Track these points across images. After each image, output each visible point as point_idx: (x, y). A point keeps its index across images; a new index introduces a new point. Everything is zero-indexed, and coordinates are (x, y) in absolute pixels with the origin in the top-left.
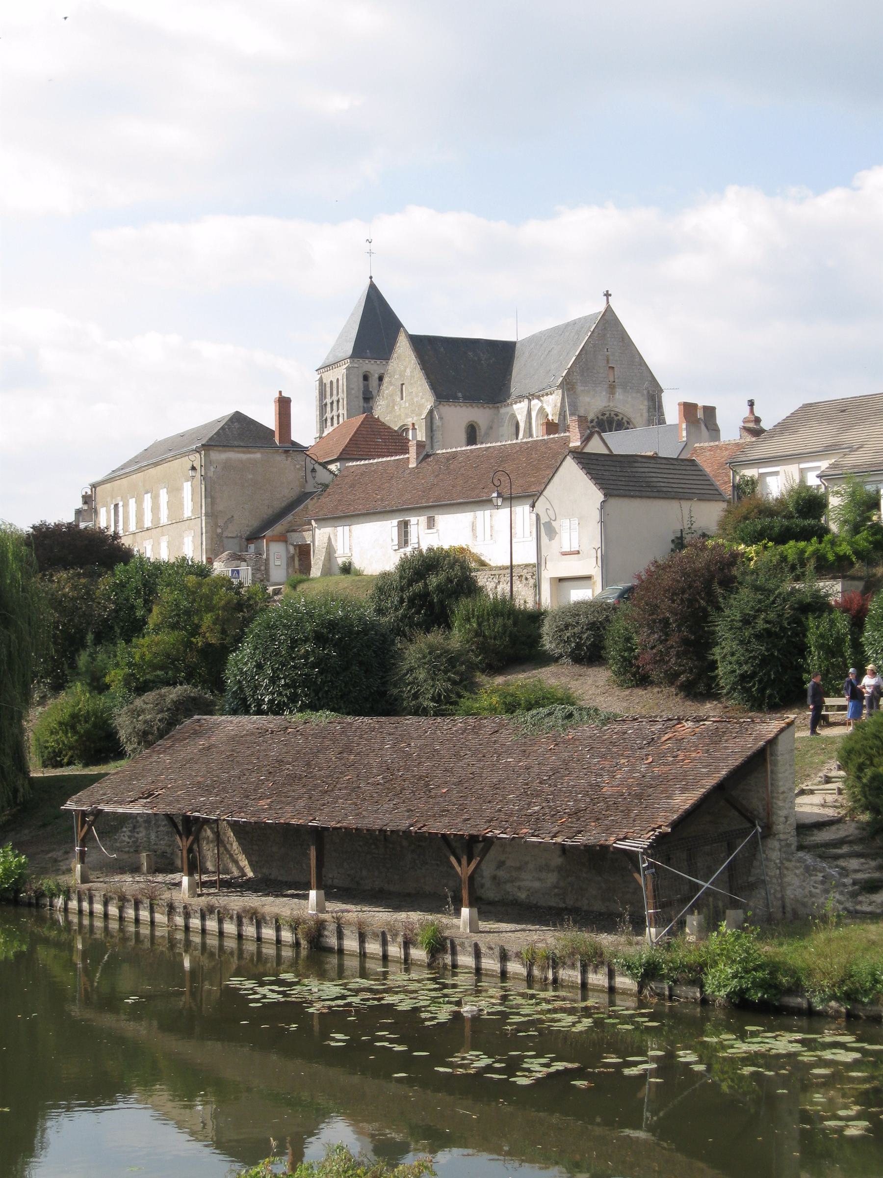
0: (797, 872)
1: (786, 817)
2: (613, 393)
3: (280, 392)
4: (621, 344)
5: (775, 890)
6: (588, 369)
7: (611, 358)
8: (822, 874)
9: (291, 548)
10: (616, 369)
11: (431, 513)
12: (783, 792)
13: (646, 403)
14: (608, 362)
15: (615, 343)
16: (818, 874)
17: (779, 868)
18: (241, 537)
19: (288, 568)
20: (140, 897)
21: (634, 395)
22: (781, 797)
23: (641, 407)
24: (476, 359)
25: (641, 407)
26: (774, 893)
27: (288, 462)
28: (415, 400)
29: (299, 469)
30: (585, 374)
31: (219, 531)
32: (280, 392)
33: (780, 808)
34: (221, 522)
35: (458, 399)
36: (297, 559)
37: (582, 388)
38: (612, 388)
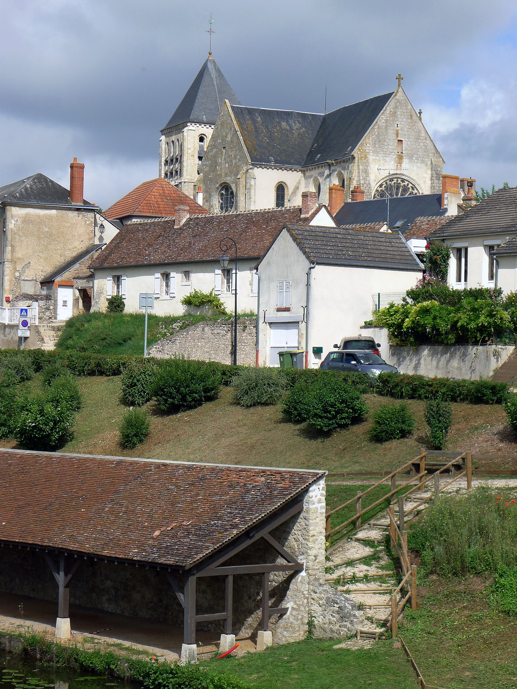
0: (321, 602)
1: (316, 557)
2: (400, 163)
3: (75, 159)
4: (409, 121)
5: (302, 616)
6: (379, 141)
7: (400, 132)
8: (338, 606)
9: (77, 292)
10: (404, 142)
11: (167, 270)
12: (314, 536)
13: (429, 172)
14: (397, 136)
15: (404, 120)
16: (335, 605)
17: (307, 598)
18: (36, 280)
19: (73, 308)
20: (469, 464)
21: (419, 165)
22: (311, 539)
23: (425, 175)
24: (288, 128)
25: (425, 175)
26: (301, 619)
27: (80, 218)
28: (234, 161)
29: (89, 225)
30: (377, 146)
31: (17, 274)
32: (75, 159)
33: (310, 549)
34: (19, 267)
35: (269, 162)
36: (81, 301)
37: (374, 158)
38: (400, 158)
